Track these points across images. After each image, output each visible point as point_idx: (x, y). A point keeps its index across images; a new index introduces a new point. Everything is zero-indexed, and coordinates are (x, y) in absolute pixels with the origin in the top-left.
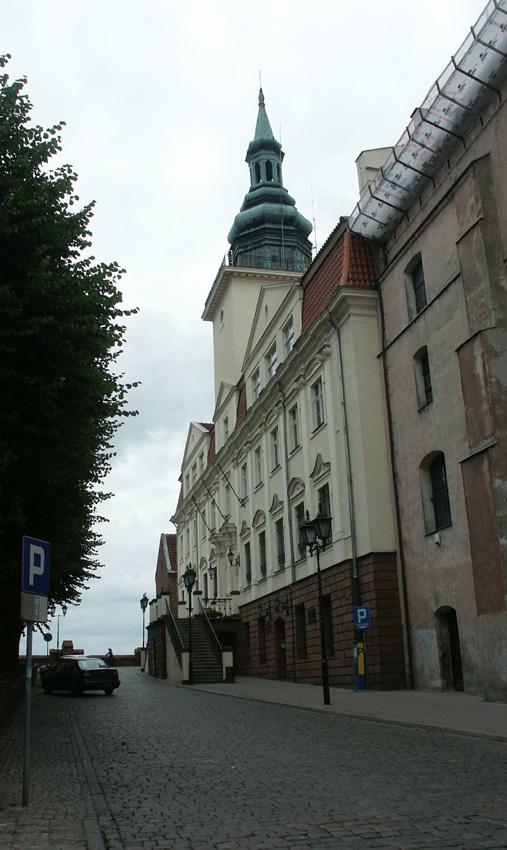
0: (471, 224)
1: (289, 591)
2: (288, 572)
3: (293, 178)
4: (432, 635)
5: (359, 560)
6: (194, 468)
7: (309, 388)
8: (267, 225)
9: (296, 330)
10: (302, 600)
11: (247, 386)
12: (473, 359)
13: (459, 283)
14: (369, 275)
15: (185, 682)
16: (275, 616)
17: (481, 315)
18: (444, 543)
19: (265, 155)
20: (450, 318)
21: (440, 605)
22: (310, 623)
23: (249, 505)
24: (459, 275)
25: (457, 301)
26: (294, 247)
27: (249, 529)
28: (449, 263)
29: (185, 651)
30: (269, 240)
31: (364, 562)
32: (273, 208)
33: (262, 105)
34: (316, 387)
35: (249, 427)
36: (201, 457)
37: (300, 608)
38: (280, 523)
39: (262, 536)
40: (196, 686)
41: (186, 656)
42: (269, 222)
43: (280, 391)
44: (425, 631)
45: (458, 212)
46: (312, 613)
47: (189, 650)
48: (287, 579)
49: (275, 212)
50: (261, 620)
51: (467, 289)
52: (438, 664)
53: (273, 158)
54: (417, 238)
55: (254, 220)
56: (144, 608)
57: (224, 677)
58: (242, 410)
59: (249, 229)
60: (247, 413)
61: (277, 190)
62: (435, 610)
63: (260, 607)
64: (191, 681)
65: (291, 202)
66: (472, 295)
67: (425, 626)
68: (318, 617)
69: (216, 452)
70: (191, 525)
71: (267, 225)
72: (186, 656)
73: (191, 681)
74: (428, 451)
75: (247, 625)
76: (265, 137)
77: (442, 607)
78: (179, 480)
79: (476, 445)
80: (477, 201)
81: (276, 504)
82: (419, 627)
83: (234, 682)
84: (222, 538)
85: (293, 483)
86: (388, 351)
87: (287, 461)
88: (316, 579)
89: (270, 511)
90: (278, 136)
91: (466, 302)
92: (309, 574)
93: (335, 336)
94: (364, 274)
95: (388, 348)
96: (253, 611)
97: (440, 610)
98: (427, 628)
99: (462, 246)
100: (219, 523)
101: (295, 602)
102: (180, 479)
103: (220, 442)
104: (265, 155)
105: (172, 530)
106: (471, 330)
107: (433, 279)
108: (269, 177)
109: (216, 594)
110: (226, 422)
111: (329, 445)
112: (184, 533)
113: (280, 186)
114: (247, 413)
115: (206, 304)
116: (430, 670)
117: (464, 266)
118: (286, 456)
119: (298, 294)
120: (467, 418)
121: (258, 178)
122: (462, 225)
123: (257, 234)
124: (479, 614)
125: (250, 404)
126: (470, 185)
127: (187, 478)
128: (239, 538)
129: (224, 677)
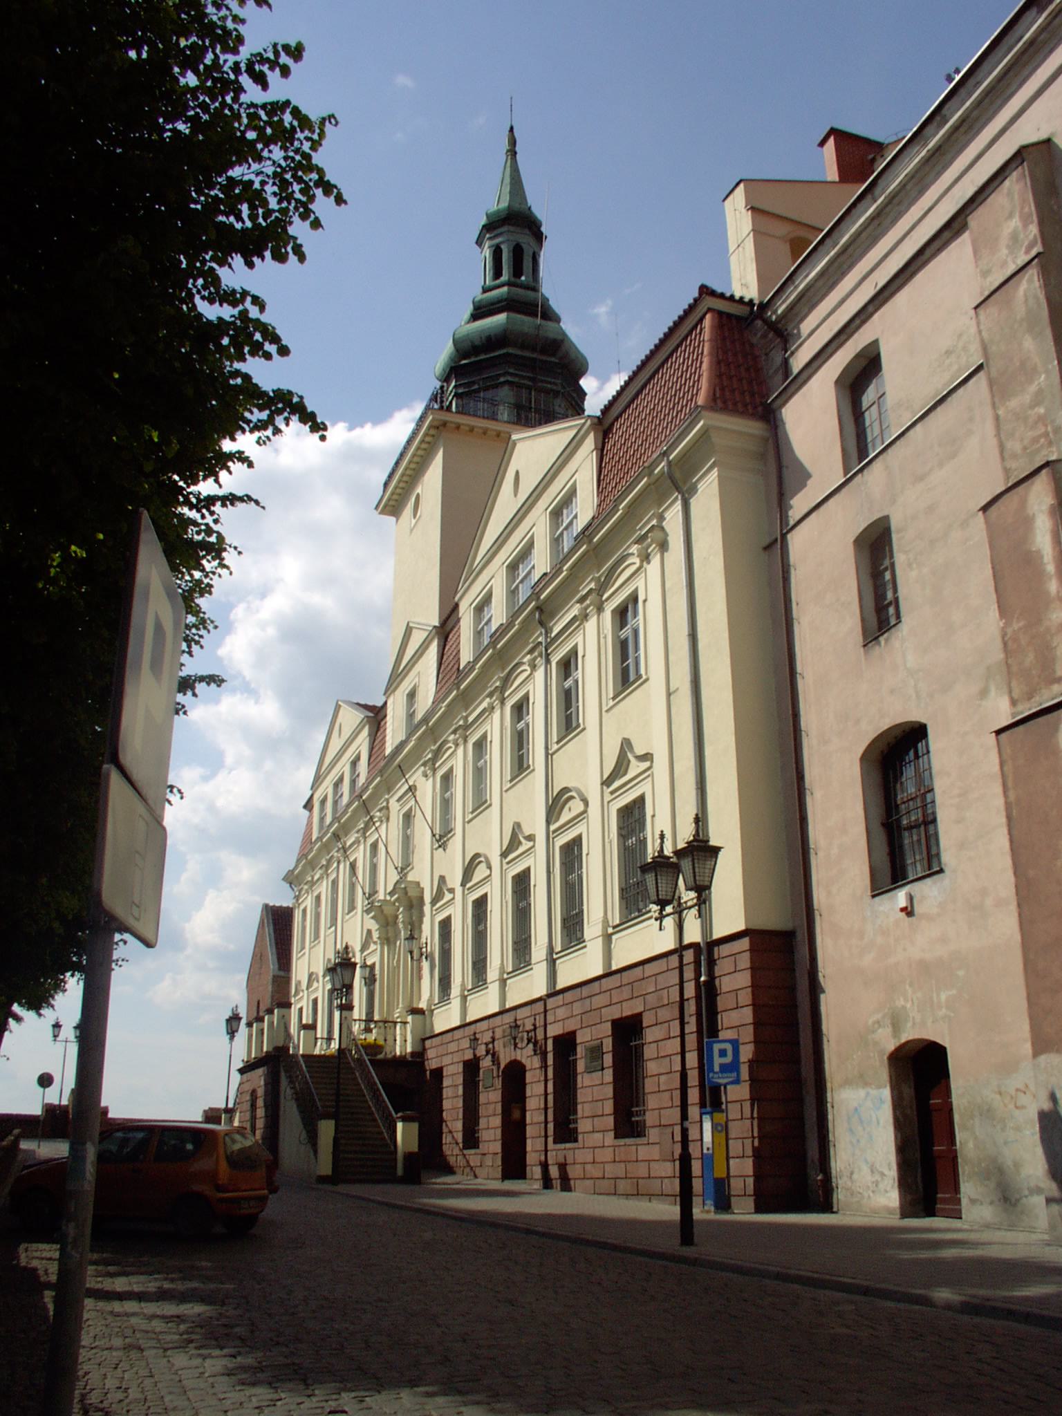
0: (1012, 268)
1: (539, 1007)
2: (455, 1003)
3: (556, 279)
4: (882, 1101)
5: (713, 944)
6: (338, 784)
7: (607, 615)
8: (511, 350)
9: (584, 509)
10: (571, 1025)
11: (462, 623)
12: (1027, 522)
13: (981, 379)
14: (752, 395)
15: (322, 1179)
16: (506, 1056)
17: (1035, 440)
18: (917, 909)
19: (515, 234)
20: (953, 455)
21: (904, 1039)
22: (589, 1070)
23: (455, 843)
24: (980, 368)
25: (971, 420)
26: (556, 394)
27: (452, 891)
28: (948, 353)
29: (327, 1116)
30: (511, 374)
31: (725, 949)
32: (525, 322)
33: (512, 153)
34: (623, 614)
35: (466, 699)
36: (354, 763)
37: (566, 1043)
38: (522, 883)
39: (481, 905)
40: (343, 1188)
41: (327, 1129)
42: (515, 345)
43: (541, 623)
44: (862, 1093)
45: (975, 252)
46: (595, 1052)
47: (335, 1116)
48: (533, 984)
49: (526, 330)
50: (471, 1068)
51: (999, 391)
52: (892, 1158)
53: (526, 240)
54: (871, 315)
55: (489, 338)
56: (232, 1033)
57: (400, 1171)
58: (448, 668)
59: (477, 354)
60: (460, 674)
61: (530, 294)
62: (891, 1046)
63: (475, 1039)
64: (334, 1179)
65: (549, 315)
66: (1013, 403)
67: (861, 1080)
68: (608, 1060)
69: (388, 751)
70: (324, 888)
71: (511, 350)
72: (327, 1129)
73: (334, 1179)
74: (886, 724)
75: (438, 1073)
76: (516, 206)
77: (908, 1042)
78: (305, 807)
79: (1030, 696)
80: (1025, 226)
81: (514, 841)
82: (847, 1082)
83: (419, 1182)
84: (401, 913)
85: (556, 804)
86: (789, 536)
87: (548, 755)
88: (674, 961)
89: (504, 855)
90: (540, 210)
91: (997, 418)
92: (453, 1026)
93: (678, 506)
94: (743, 393)
95: (788, 532)
96: (453, 1047)
97: (898, 1050)
98: (866, 1084)
99: (991, 310)
100: (387, 879)
101: (554, 1030)
102: (308, 805)
103: (394, 731)
104: (515, 234)
105: (283, 899)
106: (1007, 472)
107: (899, 389)
108: (517, 271)
109: (370, 1012)
110: (412, 695)
111: (649, 717)
112: (308, 902)
113: (535, 289)
114: (460, 674)
115: (386, 485)
116: (873, 1170)
117: (993, 349)
118: (547, 748)
119: (590, 443)
120: (1005, 644)
121: (497, 273)
122: (985, 274)
123: (492, 363)
124: (1036, 1054)
125: (466, 656)
126: (1009, 194)
127: (323, 802)
128: (427, 908)
129: (400, 1171)
